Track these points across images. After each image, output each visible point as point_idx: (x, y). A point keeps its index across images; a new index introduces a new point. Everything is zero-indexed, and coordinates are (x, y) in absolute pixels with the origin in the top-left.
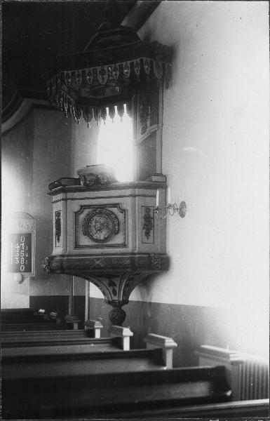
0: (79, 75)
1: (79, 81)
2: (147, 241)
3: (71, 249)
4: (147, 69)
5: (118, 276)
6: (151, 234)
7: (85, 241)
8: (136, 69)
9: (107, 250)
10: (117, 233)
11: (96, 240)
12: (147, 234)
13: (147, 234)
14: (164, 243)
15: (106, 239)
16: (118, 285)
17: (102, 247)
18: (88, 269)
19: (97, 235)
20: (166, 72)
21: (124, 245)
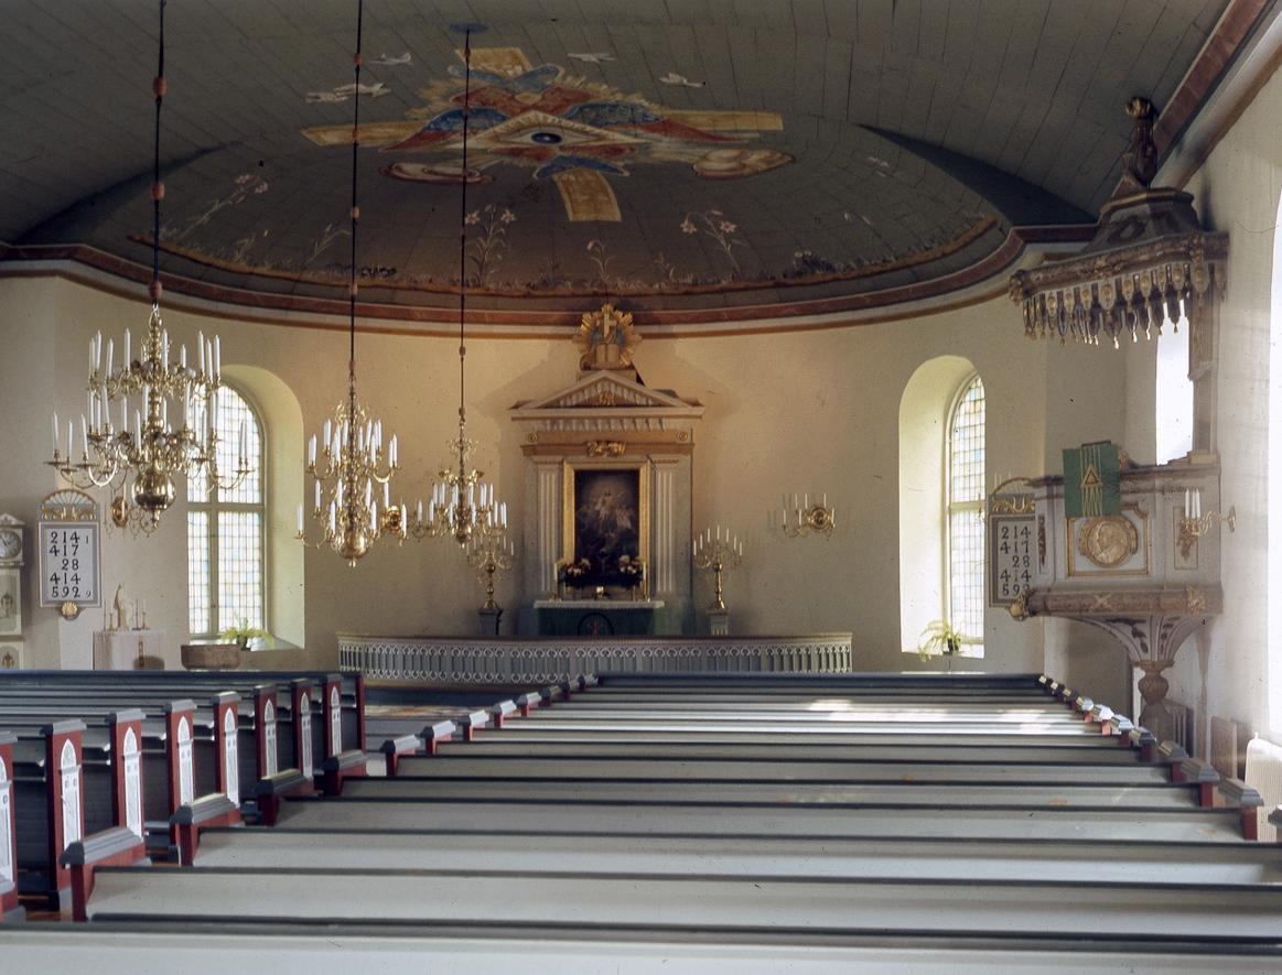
0: (1051, 298)
1: (1086, 302)
2: (1185, 565)
3: (1062, 575)
4: (1179, 281)
5: (1143, 622)
6: (1192, 551)
7: (1082, 564)
8: (1066, 302)
9: (1117, 579)
10: (1134, 551)
11: (1101, 564)
12: (1185, 553)
13: (1185, 553)
14: (1216, 563)
15: (1117, 562)
16: (1148, 635)
17: (1110, 574)
18: (1087, 610)
19: (1103, 555)
20: (1217, 276)
21: (1146, 572)
